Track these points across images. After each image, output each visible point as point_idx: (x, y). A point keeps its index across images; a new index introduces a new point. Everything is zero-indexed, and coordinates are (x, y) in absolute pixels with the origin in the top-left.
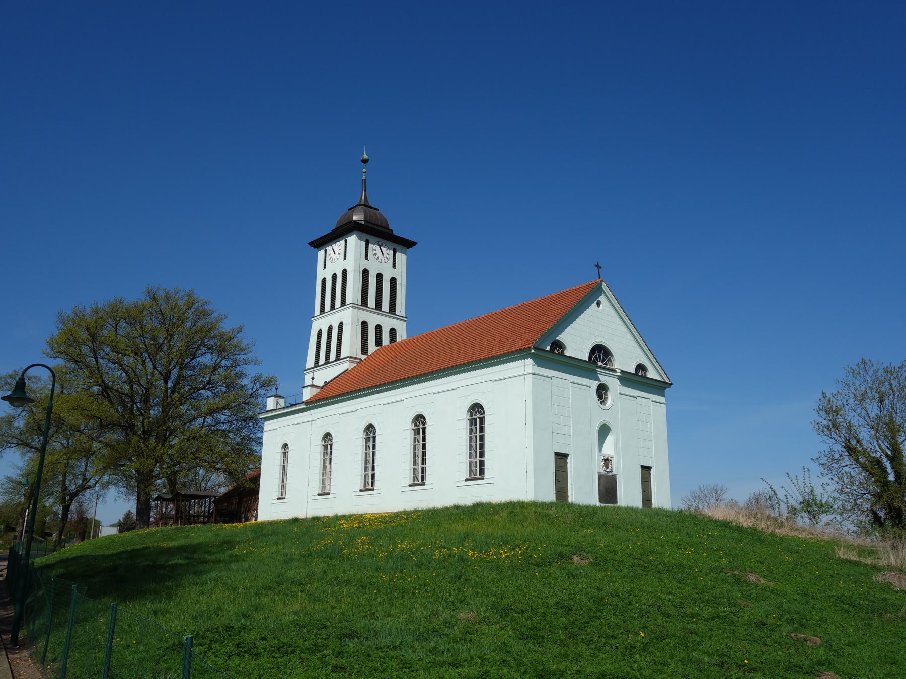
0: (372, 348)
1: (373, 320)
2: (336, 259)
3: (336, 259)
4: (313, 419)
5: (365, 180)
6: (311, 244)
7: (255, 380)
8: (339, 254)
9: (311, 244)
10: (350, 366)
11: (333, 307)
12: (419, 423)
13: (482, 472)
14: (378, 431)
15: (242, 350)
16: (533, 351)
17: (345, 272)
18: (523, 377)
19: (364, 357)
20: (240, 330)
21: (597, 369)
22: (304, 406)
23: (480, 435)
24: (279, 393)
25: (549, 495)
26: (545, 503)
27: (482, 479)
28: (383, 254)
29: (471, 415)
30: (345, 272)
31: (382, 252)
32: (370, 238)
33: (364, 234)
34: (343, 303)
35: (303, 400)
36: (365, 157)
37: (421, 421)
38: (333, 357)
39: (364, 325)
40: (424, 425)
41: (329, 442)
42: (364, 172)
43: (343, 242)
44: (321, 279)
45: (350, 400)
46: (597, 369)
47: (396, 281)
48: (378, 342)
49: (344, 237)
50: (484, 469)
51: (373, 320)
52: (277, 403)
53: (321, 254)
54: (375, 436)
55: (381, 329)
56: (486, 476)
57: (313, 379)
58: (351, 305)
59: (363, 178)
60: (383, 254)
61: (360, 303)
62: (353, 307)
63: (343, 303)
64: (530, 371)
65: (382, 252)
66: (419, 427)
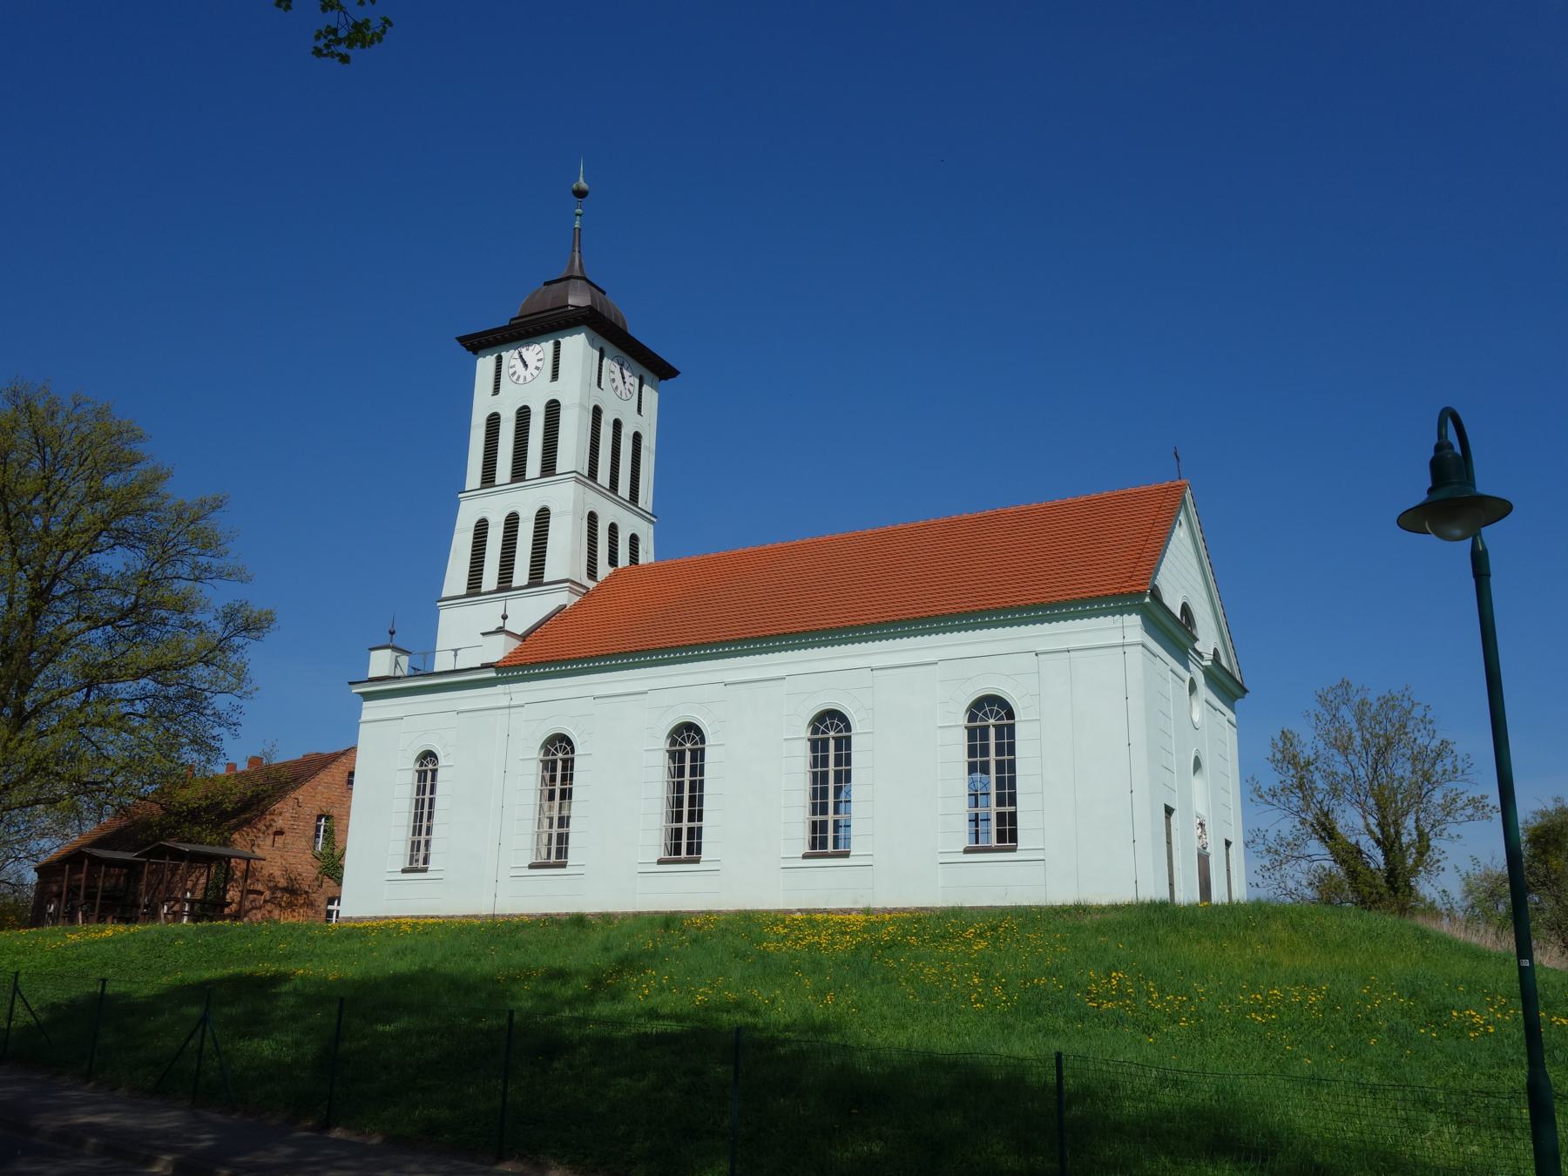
0: (604, 570)
1: (608, 512)
2: (529, 378)
3: (521, 381)
4: (513, 703)
5: (580, 230)
6: (463, 340)
7: (229, 616)
8: (537, 368)
9: (463, 340)
10: (569, 600)
11: (518, 473)
12: (556, 749)
13: (562, 852)
14: (442, 761)
15: (206, 546)
16: (1147, 600)
17: (553, 409)
18: (1120, 650)
19: (591, 585)
20: (217, 505)
21: (1190, 651)
22: (492, 674)
23: (835, 771)
24: (397, 641)
25: (1166, 896)
26: (1091, 907)
27: (563, 865)
28: (625, 383)
29: (547, 753)
30: (553, 409)
31: (623, 378)
32: (609, 347)
33: (599, 337)
34: (549, 467)
35: (369, 676)
36: (582, 184)
37: (561, 747)
38: (521, 574)
39: (592, 518)
40: (435, 765)
41: (430, 766)
42: (577, 215)
43: (548, 346)
44: (487, 415)
45: (717, 659)
46: (1190, 651)
47: (640, 441)
48: (613, 560)
49: (497, 348)
50: (566, 848)
51: (608, 512)
52: (397, 663)
53: (486, 365)
54: (437, 770)
55: (617, 533)
56: (570, 861)
57: (505, 617)
58: (574, 475)
59: (576, 226)
60: (625, 383)
61: (586, 473)
62: (577, 480)
63: (549, 467)
64: (1139, 639)
65: (623, 378)
66: (683, 748)
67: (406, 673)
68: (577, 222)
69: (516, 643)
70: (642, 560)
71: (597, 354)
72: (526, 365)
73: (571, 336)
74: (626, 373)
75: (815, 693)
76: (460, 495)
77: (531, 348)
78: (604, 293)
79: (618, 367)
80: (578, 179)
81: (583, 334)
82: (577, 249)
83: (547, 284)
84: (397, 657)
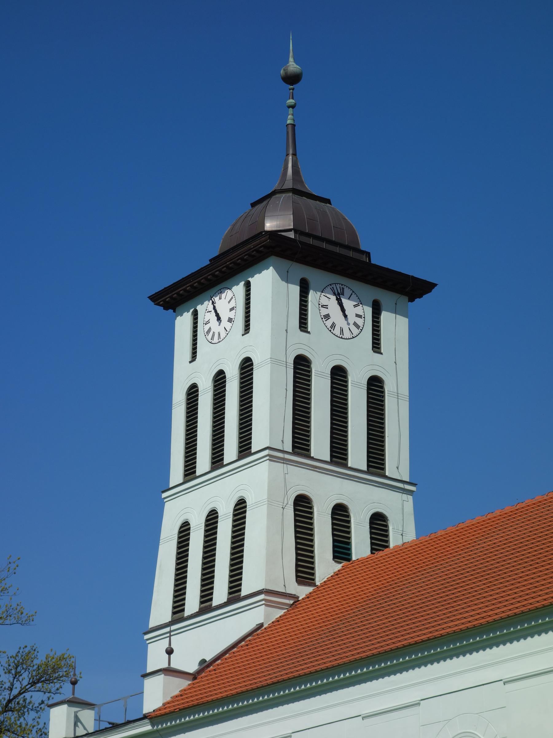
5: (294, 126)
6: (155, 298)
9: (155, 298)
10: (267, 616)
19: (303, 591)
24: (81, 693)
31: (343, 310)
36: (293, 66)
42: (289, 107)
43: (239, 289)
47: (382, 387)
52: (77, 721)
58: (266, 452)
60: (345, 316)
65: (343, 310)
67: (91, 730)
68: (290, 117)
69: (184, 684)
70: (394, 541)
71: (295, 290)
72: (219, 319)
73: (260, 273)
74: (348, 304)
75: (451, 720)
76: (164, 495)
77: (223, 295)
78: (328, 201)
79: (333, 298)
80: (288, 62)
81: (271, 268)
82: (291, 152)
83: (253, 205)
84: (76, 713)
